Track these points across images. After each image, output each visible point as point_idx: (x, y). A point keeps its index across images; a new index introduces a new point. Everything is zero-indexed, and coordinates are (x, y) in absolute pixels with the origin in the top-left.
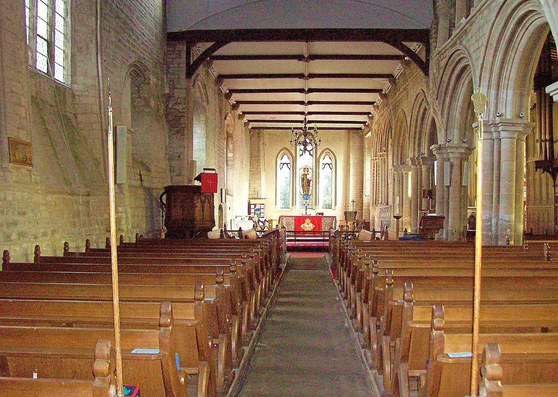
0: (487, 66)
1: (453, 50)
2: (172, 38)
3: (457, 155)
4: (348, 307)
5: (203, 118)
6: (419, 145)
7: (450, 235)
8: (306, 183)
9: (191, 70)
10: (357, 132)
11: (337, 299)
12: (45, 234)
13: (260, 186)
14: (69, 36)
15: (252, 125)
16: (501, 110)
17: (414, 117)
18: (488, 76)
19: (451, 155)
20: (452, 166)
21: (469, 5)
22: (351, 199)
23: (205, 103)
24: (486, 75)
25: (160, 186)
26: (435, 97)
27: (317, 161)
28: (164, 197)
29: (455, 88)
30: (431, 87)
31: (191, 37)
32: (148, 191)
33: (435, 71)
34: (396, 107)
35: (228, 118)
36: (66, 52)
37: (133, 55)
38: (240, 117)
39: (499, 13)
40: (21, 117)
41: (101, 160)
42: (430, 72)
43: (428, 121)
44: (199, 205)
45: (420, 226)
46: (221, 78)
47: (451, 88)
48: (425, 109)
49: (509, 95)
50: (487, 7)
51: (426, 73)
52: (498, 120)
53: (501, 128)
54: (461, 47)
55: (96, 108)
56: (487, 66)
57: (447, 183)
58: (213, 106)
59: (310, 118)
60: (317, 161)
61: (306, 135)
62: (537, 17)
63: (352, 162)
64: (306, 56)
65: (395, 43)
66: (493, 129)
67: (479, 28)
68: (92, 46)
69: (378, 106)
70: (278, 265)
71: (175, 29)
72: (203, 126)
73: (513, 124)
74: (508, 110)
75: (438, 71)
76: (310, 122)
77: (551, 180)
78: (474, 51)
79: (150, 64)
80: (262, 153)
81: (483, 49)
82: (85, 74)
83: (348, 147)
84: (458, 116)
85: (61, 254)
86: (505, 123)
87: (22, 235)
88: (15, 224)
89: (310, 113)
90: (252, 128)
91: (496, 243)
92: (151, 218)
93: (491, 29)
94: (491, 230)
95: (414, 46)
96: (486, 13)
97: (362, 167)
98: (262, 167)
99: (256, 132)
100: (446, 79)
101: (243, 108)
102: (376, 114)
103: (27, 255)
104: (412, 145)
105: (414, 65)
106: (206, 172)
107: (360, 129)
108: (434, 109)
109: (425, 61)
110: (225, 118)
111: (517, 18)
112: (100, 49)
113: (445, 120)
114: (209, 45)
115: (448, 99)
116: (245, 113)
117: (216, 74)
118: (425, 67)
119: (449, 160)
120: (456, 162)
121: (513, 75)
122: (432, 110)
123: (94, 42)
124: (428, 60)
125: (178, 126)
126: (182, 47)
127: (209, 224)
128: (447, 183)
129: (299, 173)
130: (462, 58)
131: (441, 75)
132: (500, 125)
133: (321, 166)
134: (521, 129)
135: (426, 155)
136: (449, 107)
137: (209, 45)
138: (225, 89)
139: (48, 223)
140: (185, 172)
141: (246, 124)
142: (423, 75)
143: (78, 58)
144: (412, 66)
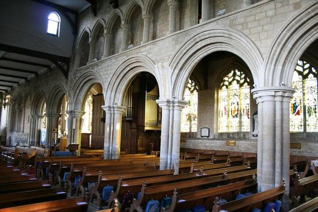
1: (88, 70)
16: (116, 101)
20: (77, 120)
24: (111, 86)
42: (69, 77)
47: (80, 86)
49: (120, 96)
51: (67, 77)
65: (55, 62)
115: (78, 91)
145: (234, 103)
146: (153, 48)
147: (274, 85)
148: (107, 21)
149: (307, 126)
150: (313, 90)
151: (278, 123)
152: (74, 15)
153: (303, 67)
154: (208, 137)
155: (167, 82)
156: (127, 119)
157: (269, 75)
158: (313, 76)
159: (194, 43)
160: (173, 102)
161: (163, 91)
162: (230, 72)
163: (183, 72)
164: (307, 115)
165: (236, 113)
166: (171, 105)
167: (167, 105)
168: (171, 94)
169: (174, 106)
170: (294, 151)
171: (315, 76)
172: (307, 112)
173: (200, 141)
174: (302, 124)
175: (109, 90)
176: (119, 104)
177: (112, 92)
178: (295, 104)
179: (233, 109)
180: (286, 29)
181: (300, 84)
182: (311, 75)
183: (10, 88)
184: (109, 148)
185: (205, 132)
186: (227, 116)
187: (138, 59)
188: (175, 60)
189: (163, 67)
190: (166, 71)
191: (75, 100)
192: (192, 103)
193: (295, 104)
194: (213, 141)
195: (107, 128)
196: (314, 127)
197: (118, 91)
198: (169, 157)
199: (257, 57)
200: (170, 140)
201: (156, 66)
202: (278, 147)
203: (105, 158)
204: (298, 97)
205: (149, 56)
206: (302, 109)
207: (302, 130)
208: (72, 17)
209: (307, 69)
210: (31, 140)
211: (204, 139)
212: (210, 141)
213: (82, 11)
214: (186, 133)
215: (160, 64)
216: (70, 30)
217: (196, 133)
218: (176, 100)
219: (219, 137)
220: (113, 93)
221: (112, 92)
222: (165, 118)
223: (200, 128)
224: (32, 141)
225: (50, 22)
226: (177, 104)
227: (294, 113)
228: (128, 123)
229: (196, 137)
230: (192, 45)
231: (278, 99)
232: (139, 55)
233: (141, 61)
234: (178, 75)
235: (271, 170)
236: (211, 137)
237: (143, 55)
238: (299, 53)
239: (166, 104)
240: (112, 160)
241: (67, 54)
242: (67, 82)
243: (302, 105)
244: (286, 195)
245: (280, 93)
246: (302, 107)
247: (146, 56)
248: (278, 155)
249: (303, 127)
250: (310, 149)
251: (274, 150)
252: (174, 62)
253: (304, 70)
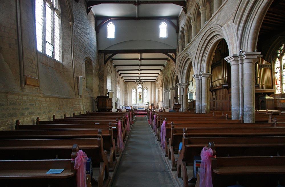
1: (185, 54)
2: (100, 52)
5: (110, 77)
7: (183, 110)
8: (140, 96)
9: (106, 62)
10: (154, 82)
12: (44, 112)
14: (61, 46)
15: (125, 81)
16: (202, 70)
17: (171, 76)
18: (198, 60)
19: (183, 86)
20: (184, 89)
21: (220, 3)
23: (111, 73)
24: (197, 59)
25: (96, 96)
26: (178, 69)
27: (143, 90)
28: (97, 99)
31: (106, 52)
32: (92, 98)
34: (165, 74)
36: (60, 51)
37: (86, 55)
38: (122, 78)
40: (33, 68)
41: (74, 87)
43: (175, 77)
44: (107, 102)
45: (174, 107)
46: (115, 66)
47: (183, 66)
48: (175, 73)
49: (204, 65)
50: (197, 38)
52: (201, 73)
53: (202, 76)
55: (71, 70)
57: (182, 94)
58: (113, 73)
60: (143, 90)
62: (219, 36)
63: (152, 90)
64: (140, 65)
66: (199, 76)
67: (194, 45)
68: (70, 50)
69: (159, 75)
70: (132, 120)
71: (101, 50)
72: (110, 79)
73: (206, 75)
74: (204, 70)
76: (141, 77)
77: (211, 93)
78: (192, 53)
79: (92, 59)
82: (67, 59)
84: (185, 74)
85: (72, 116)
86: (203, 74)
87: (31, 113)
88: (28, 109)
89: (141, 74)
91: (202, 113)
92: (92, 106)
93: (199, 44)
94: (199, 108)
95: (171, 54)
97: (155, 91)
98: (128, 92)
99: (126, 83)
101: (122, 75)
102: (159, 78)
103: (34, 121)
104: (170, 83)
107: (154, 81)
108: (178, 73)
109: (175, 58)
110: (117, 78)
111: (209, 39)
112: (73, 51)
113: (181, 76)
114: (111, 54)
116: (123, 77)
117: (114, 65)
118: (175, 60)
119: (182, 88)
120: (185, 88)
122: (177, 73)
123: (70, 48)
124: (176, 59)
125: (102, 80)
126: (103, 55)
127: (110, 108)
128: (182, 94)
129: (138, 94)
131: (180, 62)
132: (239, 57)
133: (144, 92)
134: (209, 76)
135: (174, 87)
137: (111, 54)
138: (117, 69)
139: (47, 108)
140: (105, 93)
141: (122, 78)
143: (65, 53)
146: (221, 14)
148: (192, 13)
152: (176, 20)
155: (234, 39)
160: (241, 56)
161: (231, 48)
163: (249, 24)
167: (234, 60)
169: (242, 60)
176: (205, 72)
180: (241, 3)
187: (211, 30)
188: (239, 14)
189: (228, 26)
192: (254, 52)
195: (56, 4)
197: (202, 62)
198: (240, 109)
200: (240, 92)
201: (223, 28)
203: (197, 113)
208: (174, 21)
210: (165, 105)
213: (180, 15)
222: (234, 73)
224: (166, 106)
226: (245, 57)
228: (226, 89)
233: (213, 31)
234: (244, 29)
237: (214, 24)
238: (262, 4)
239: (233, 59)
247: (216, 24)
252: (238, 17)
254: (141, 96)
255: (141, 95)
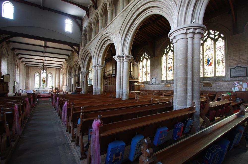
0: (96, 52)
1: (86, 49)
3: (85, 74)
4: (58, 115)
6: (76, 72)
8: (44, 81)
11: (54, 112)
13: (29, 81)
16: (98, 63)
20: (84, 76)
22: (56, 85)
24: (95, 55)
26: (81, 60)
27: (47, 75)
29: (86, 58)
30: (80, 58)
33: (81, 54)
35: (17, 62)
38: (22, 62)
39: (100, 39)
42: (79, 54)
49: (100, 60)
51: (78, 54)
52: (98, 65)
53: (98, 67)
54: (88, 48)
56: (96, 52)
57: (83, 80)
59: (45, 62)
60: (47, 75)
61: (44, 67)
63: (57, 76)
64: (44, 52)
69: (64, 63)
72: (7, 62)
73: (101, 67)
75: (82, 54)
76: (45, 63)
77: (104, 80)
80: (30, 72)
81: (95, 48)
83: (56, 72)
86: (99, 66)
89: (45, 60)
90: (27, 66)
94: (96, 91)
95: (75, 47)
96: (96, 40)
98: (30, 76)
100: (84, 56)
102: (64, 65)
105: (75, 52)
106: (6, 75)
110: (16, 61)
115: (84, 61)
117: (12, 47)
118: (78, 53)
120: (85, 76)
121: (102, 55)
122: (80, 63)
128: (83, 80)
129: (42, 79)
130: (88, 51)
136: (84, 63)
141: (24, 64)
142: (78, 55)
144: (74, 53)
145: (170, 63)
147: (186, 24)
149: (217, 72)
150: (221, 48)
151: (189, 55)
153: (214, 35)
154: (155, 83)
156: (112, 75)
157: (181, 18)
158: (221, 39)
159: (132, 14)
160: (122, 56)
162: (168, 46)
163: (128, 37)
164: (217, 65)
165: (171, 68)
166: (122, 58)
167: (119, 59)
168: (121, 52)
169: (123, 60)
170: (207, 88)
171: (223, 38)
172: (217, 63)
173: (151, 85)
174: (213, 71)
175: (95, 57)
176: (100, 64)
177: (96, 57)
178: (208, 59)
179: (169, 67)
181: (212, 46)
182: (220, 39)
183: (61, 65)
184: (95, 89)
185: (154, 81)
186: (166, 71)
190: (118, 38)
191: (83, 66)
193: (208, 59)
194: (158, 85)
196: (222, 72)
199: (173, 7)
202: (189, 76)
204: (211, 54)
205: (110, 31)
206: (213, 62)
207: (213, 75)
208: (79, 21)
209: (217, 35)
210: (69, 89)
211: (153, 84)
212: (156, 85)
214: (144, 82)
215: (114, 34)
216: (78, 28)
217: (149, 82)
218: (124, 55)
219: (161, 83)
220: (97, 59)
221: (96, 57)
223: (151, 78)
224: (70, 90)
225: (66, 24)
226: (125, 58)
227: (207, 64)
229: (149, 83)
230: (131, 16)
231: (190, 36)
232: (106, 32)
235: (183, 94)
236: (157, 83)
240: (97, 95)
241: (78, 42)
242: (79, 57)
243: (213, 59)
244: (197, 115)
245: (191, 30)
246: (213, 60)
248: (189, 82)
249: (214, 73)
250: (219, 87)
251: (186, 79)
252: (122, 31)
253: (215, 36)
254: (44, 80)
255: (45, 79)
